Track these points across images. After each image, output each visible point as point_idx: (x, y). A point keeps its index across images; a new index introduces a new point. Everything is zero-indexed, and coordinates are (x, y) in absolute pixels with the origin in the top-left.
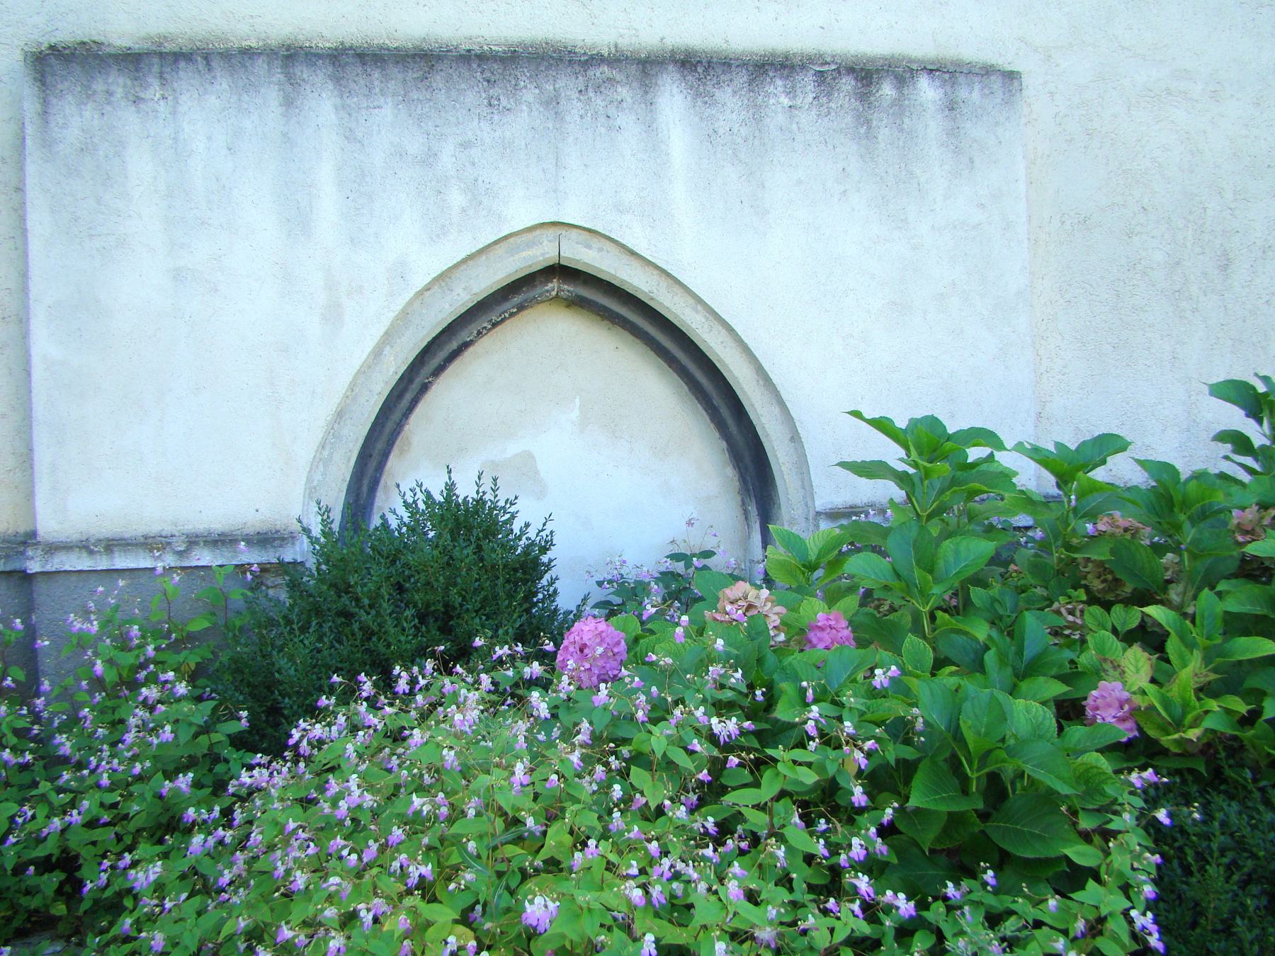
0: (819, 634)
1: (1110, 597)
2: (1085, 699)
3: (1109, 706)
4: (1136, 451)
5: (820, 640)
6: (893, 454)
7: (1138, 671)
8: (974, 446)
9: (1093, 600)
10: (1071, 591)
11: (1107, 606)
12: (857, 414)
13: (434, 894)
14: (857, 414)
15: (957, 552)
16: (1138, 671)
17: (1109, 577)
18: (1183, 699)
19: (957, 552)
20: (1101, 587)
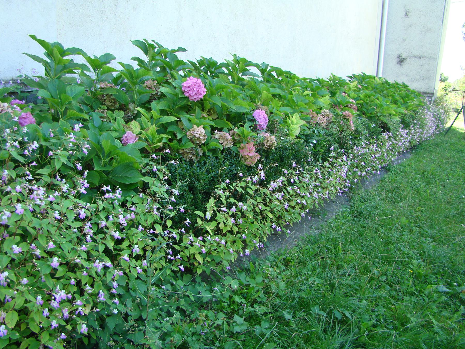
0: (24, 120)
1: (112, 108)
2: (122, 137)
3: (132, 138)
4: (118, 60)
5: (25, 122)
6: (41, 52)
7: (136, 128)
8: (78, 54)
9: (108, 109)
10: (101, 106)
11: (113, 111)
12: (33, 37)
13: (90, 160)
14: (33, 37)
15: (71, 91)
16: (136, 128)
17: (113, 101)
18: (152, 135)
19: (71, 91)
20: (110, 104)
